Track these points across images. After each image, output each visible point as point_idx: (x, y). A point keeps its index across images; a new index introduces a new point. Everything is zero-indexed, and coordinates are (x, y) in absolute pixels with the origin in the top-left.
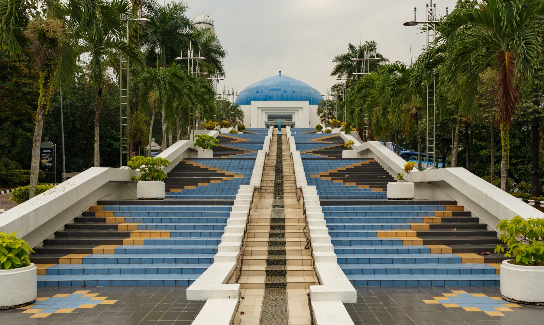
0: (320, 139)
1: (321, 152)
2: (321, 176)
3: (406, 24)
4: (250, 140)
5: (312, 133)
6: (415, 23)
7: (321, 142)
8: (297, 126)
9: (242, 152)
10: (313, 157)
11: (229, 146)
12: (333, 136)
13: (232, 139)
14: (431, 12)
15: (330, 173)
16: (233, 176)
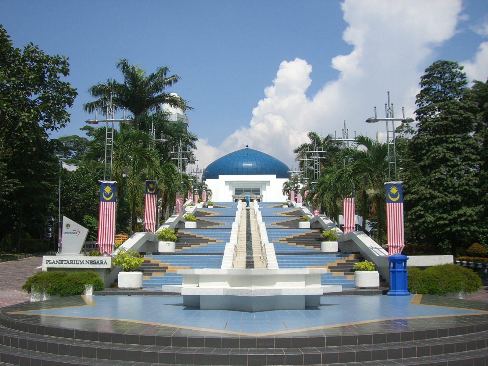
0: (284, 212)
1: (283, 224)
2: (280, 241)
3: (368, 121)
4: (222, 214)
5: (276, 207)
6: (376, 121)
7: (285, 215)
8: (264, 200)
9: (218, 224)
10: (305, 251)
11: (206, 219)
12: (295, 210)
13: (206, 213)
14: (389, 111)
15: (287, 239)
16: (215, 241)
